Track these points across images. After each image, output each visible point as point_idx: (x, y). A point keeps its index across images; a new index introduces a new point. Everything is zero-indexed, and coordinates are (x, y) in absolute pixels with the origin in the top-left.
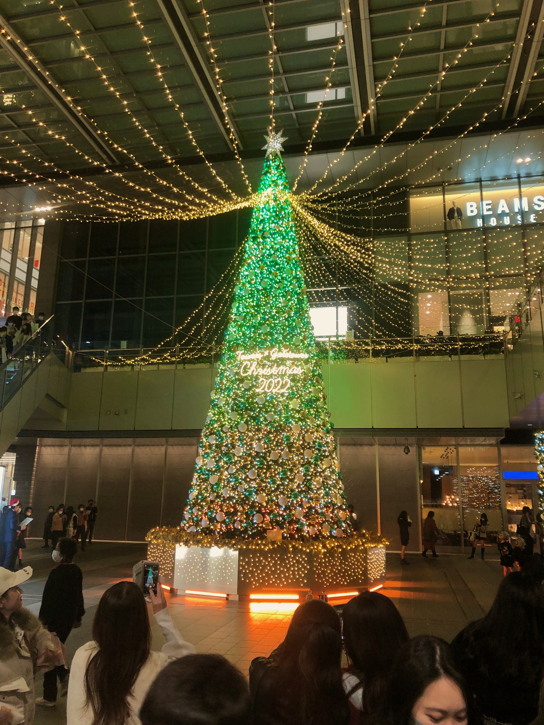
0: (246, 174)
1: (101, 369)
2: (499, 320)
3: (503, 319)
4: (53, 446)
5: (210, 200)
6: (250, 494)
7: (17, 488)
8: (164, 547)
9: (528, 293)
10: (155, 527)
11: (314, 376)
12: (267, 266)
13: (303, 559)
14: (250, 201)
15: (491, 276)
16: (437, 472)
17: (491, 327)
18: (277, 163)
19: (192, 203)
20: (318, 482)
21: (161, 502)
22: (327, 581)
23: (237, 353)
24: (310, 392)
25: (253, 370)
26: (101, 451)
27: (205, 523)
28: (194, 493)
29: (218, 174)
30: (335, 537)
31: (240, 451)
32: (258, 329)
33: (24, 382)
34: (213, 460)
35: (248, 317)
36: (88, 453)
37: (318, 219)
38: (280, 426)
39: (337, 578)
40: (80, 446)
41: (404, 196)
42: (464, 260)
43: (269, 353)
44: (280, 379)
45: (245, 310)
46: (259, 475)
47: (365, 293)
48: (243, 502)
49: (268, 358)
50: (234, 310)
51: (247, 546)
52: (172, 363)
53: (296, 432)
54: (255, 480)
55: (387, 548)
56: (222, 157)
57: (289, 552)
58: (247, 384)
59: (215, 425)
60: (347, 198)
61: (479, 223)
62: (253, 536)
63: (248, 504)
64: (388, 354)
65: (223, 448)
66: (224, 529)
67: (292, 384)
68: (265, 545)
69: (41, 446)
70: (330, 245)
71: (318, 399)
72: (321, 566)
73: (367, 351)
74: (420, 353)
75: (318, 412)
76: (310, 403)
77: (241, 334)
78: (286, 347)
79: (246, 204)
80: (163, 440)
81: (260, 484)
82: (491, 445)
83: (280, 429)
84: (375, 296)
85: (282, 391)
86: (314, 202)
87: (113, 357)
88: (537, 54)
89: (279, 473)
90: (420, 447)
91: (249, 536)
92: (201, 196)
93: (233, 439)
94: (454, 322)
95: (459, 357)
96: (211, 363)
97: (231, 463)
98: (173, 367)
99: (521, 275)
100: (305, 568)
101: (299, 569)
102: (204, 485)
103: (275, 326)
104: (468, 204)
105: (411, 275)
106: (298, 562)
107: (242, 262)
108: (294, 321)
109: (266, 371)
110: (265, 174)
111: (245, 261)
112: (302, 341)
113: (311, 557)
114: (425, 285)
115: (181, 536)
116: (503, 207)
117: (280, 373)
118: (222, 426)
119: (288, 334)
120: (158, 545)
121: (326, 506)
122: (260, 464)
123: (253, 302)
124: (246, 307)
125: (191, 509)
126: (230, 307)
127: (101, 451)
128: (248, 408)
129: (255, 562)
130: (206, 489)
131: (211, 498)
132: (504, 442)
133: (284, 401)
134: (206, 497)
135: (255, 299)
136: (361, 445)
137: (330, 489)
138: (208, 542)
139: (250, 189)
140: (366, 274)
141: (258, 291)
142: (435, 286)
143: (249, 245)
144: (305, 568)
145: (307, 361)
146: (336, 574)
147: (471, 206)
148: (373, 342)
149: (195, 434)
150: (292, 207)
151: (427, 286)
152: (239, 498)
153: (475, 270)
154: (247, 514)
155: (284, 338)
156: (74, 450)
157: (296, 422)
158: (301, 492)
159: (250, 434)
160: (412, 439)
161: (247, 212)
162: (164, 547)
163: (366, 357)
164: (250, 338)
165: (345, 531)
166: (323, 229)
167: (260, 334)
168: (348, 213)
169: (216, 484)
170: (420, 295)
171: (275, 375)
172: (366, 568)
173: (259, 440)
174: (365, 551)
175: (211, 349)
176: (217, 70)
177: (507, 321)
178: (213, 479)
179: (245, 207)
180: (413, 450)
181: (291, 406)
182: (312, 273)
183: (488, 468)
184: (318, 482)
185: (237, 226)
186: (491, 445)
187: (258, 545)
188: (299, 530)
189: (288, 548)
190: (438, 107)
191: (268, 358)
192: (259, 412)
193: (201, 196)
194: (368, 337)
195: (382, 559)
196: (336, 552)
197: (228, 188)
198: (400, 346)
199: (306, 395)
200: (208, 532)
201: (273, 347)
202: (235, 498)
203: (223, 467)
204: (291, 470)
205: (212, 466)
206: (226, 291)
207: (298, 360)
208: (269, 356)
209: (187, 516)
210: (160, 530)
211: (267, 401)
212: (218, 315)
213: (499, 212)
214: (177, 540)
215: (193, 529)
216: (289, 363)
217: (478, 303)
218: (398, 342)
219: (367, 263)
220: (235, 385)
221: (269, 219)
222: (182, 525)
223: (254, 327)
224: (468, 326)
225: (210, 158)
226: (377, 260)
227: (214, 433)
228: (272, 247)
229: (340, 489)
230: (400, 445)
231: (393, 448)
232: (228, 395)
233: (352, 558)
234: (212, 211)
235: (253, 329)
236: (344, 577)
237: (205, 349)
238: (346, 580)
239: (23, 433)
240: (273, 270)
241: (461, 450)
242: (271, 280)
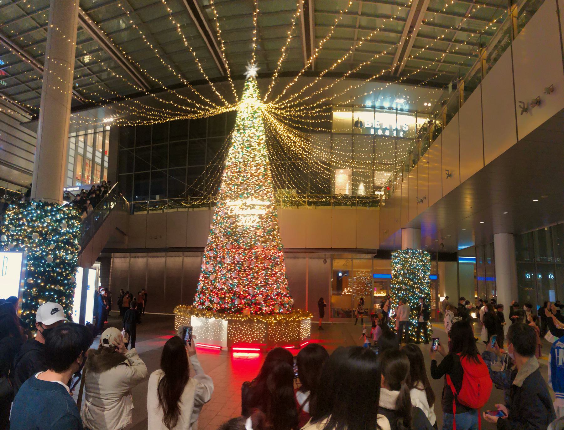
0: (235, 89)
1: (145, 212)
2: (379, 188)
3: (381, 188)
4: (121, 257)
5: (211, 106)
6: (234, 287)
7: (102, 282)
8: (184, 317)
9: (396, 176)
10: (179, 305)
11: (272, 215)
13: (263, 327)
14: (236, 107)
15: (377, 163)
16: (340, 274)
17: (374, 192)
18: (254, 83)
19: (200, 108)
20: (273, 280)
21: (181, 290)
22: (276, 340)
23: (226, 201)
24: (270, 225)
25: (236, 211)
26: (147, 260)
27: (207, 303)
28: (200, 286)
29: (217, 90)
30: (282, 313)
31: (228, 260)
32: (240, 186)
33: (105, 220)
35: (233, 179)
36: (140, 262)
37: (278, 119)
38: (251, 245)
39: (283, 338)
40: (135, 257)
41: (330, 110)
42: (363, 152)
45: (232, 174)
47: (305, 167)
48: (230, 291)
50: (225, 175)
51: (232, 318)
52: (185, 207)
53: (260, 250)
54: (236, 278)
55: (312, 319)
56: (220, 79)
57: (254, 322)
58: (232, 220)
59: (213, 245)
60: (297, 108)
61: (372, 132)
62: (235, 312)
63: (232, 293)
64: (316, 204)
65: (218, 259)
66: (219, 307)
67: (260, 220)
68: (242, 318)
69: (114, 257)
70: (284, 136)
71: (274, 230)
72: (273, 331)
73: (304, 201)
74: (335, 204)
75: (274, 237)
76: (269, 232)
77: (229, 189)
78: (256, 197)
79: (234, 109)
80: (181, 253)
82: (369, 259)
83: (251, 247)
84: (311, 169)
86: (276, 109)
87: (153, 205)
90: (332, 259)
91: (233, 312)
92: (205, 104)
94: (355, 187)
96: (209, 207)
98: (186, 210)
99: (393, 164)
100: (264, 332)
101: (260, 333)
105: (334, 158)
106: (260, 328)
107: (229, 145)
108: (261, 182)
109: (244, 212)
110: (246, 90)
111: (232, 144)
112: (266, 194)
113: (268, 325)
114: (341, 164)
115: (194, 311)
118: (217, 245)
119: (257, 190)
120: (181, 316)
121: (276, 295)
124: (232, 173)
125: (199, 295)
126: (222, 173)
127: (147, 260)
128: (233, 234)
129: (236, 328)
130: (207, 283)
131: (211, 288)
132: (375, 257)
133: (254, 231)
134: (208, 288)
136: (298, 258)
137: (280, 285)
138: (209, 315)
139: (237, 99)
140: (306, 155)
141: (240, 162)
142: (346, 165)
143: (235, 134)
144: (264, 332)
145: (268, 207)
146: (282, 336)
148: (308, 196)
149: (200, 250)
150: (262, 112)
151: (341, 165)
153: (369, 158)
154: (231, 298)
155: (255, 192)
156: (132, 260)
157: (261, 243)
158: (262, 286)
159: (234, 250)
160: (328, 255)
161: (234, 113)
162: (184, 317)
163: (303, 205)
164: (234, 192)
165: (288, 310)
166: (280, 128)
167: (241, 189)
168: (297, 117)
169: (214, 280)
170: (337, 170)
172: (299, 331)
173: (239, 254)
174: (299, 322)
175: (209, 199)
176: (218, 24)
177: (383, 189)
178: (212, 278)
179: (233, 111)
180: (328, 261)
181: (258, 234)
182: (273, 153)
183: (367, 272)
184: (273, 280)
185: (227, 122)
186: (369, 259)
187: (238, 317)
188: (261, 309)
189: (254, 320)
192: (239, 237)
193: (205, 104)
194: (305, 193)
195: (309, 326)
196: (282, 322)
197: (223, 98)
198: (324, 200)
199: (267, 227)
200: (209, 309)
201: (248, 197)
203: (218, 270)
204: (257, 273)
205: (211, 269)
206: (219, 163)
207: (263, 206)
208: (245, 203)
209: (197, 299)
210: (182, 307)
211: (244, 230)
212: (214, 178)
214: (192, 313)
215: (201, 307)
216: (257, 207)
217: (368, 178)
218: (323, 197)
219: (307, 148)
221: (247, 118)
222: (194, 304)
223: (237, 185)
224: (361, 190)
225: (212, 80)
226: (313, 147)
227: (213, 250)
228: (249, 136)
229: (286, 284)
230: (321, 258)
231: (317, 260)
232: (221, 227)
233: (292, 326)
234: (211, 113)
236: (286, 337)
237: (206, 198)
238: (288, 339)
239: (105, 250)
240: (249, 150)
241: (354, 261)
242: (248, 156)
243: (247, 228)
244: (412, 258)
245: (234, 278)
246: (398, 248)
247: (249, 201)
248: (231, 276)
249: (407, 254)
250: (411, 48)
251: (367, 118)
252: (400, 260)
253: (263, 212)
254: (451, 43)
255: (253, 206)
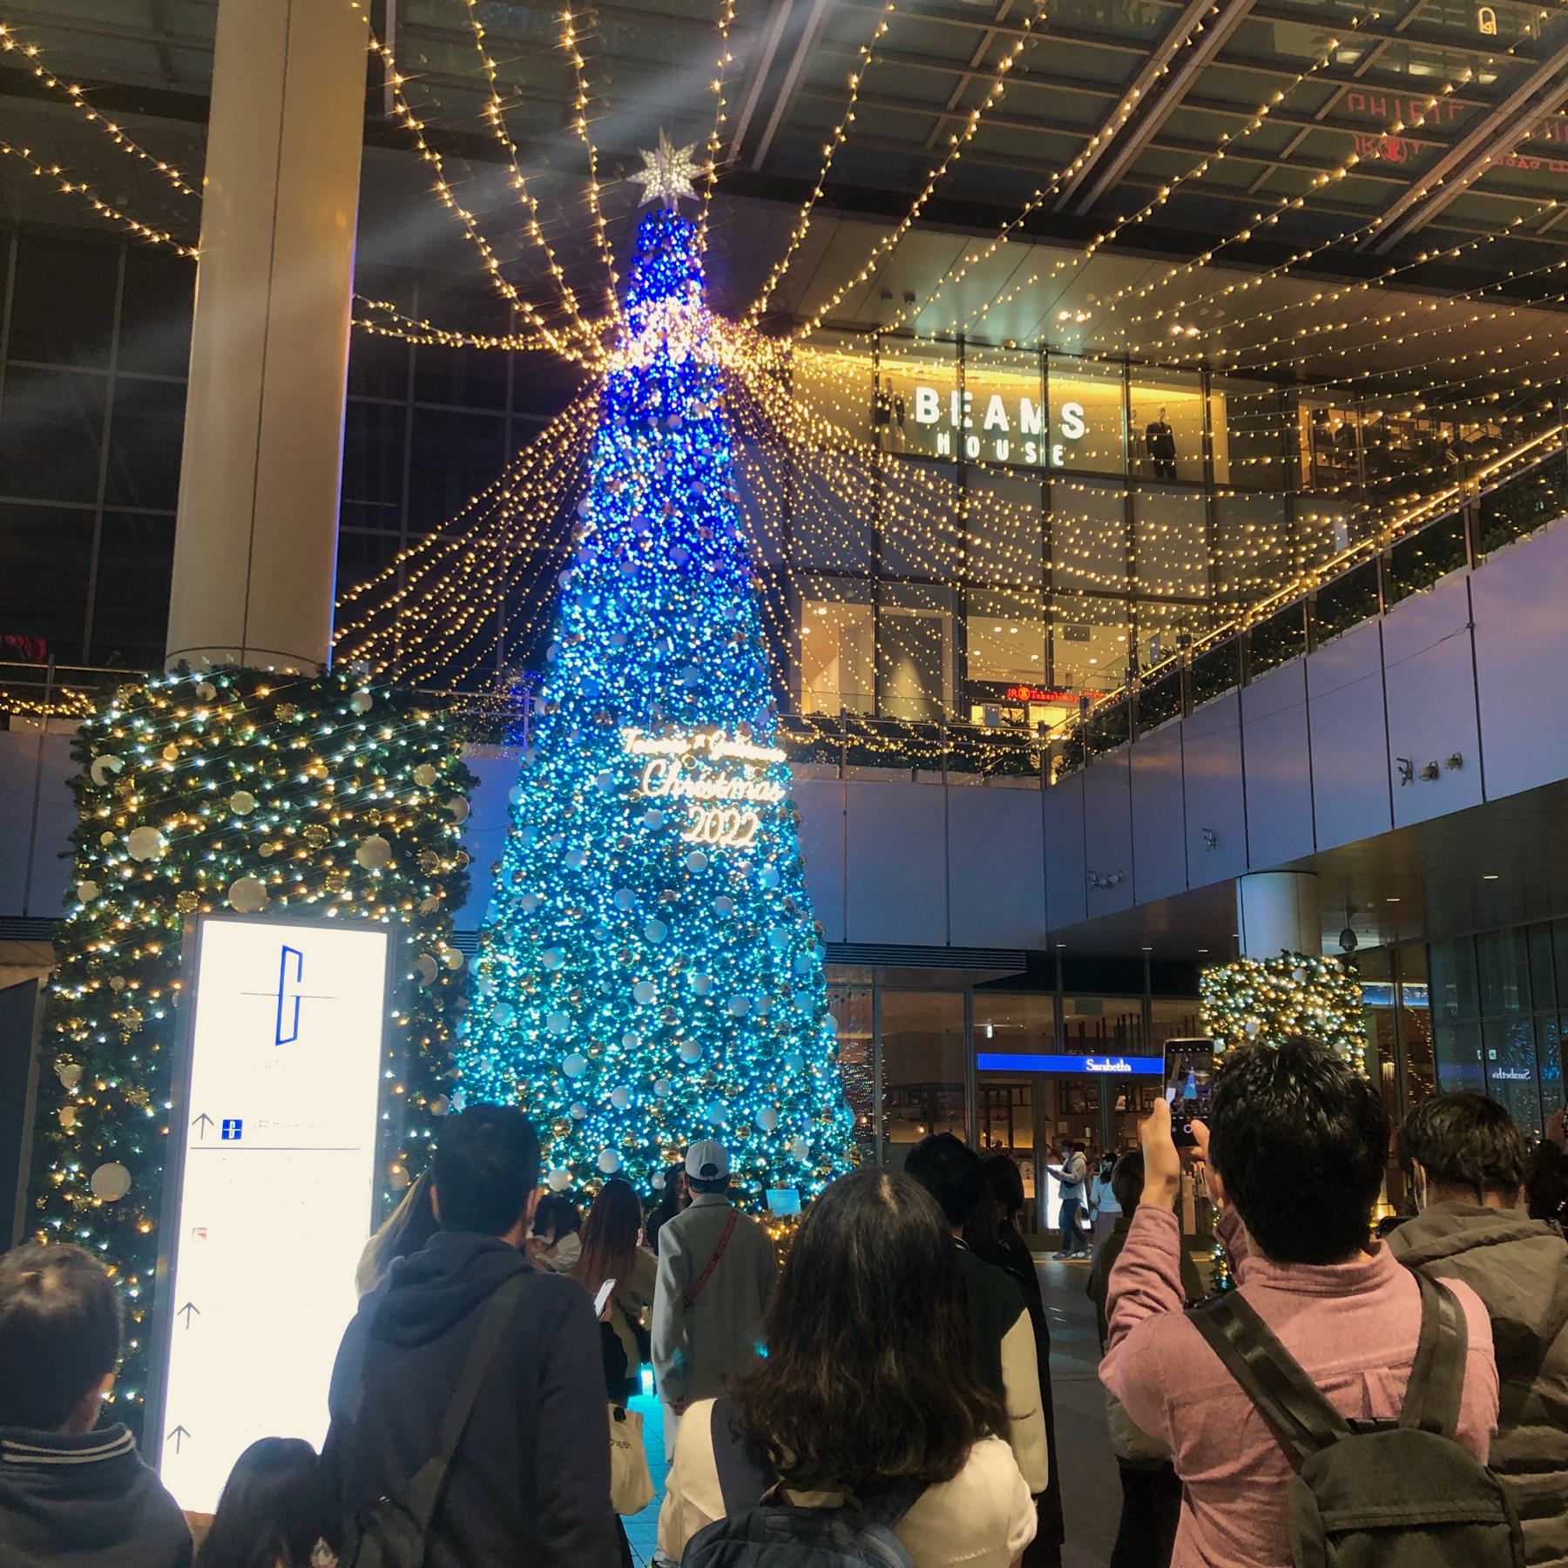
12: (682, 507)
25: (673, 784)
34: (565, 1013)
43: (707, 742)
44: (734, 811)
46: (706, 1055)
49: (702, 753)
54: (696, 1066)
63: (685, 1129)
81: (711, 1076)
85: (739, 844)
88: (1184, 92)
89: (752, 1051)
93: (627, 961)
95: (944, 777)
97: (628, 1022)
102: (537, 1079)
103: (713, 672)
104: (921, 392)
116: (996, 416)
117: (733, 797)
122: (707, 1027)
123: (651, 598)
135: (658, 594)
147: (927, 398)
152: (660, 1112)
157: (778, 924)
167: (679, 690)
171: (723, 801)
173: (699, 964)
190: (930, 145)
191: (702, 753)
202: (649, 1112)
211: (711, 865)
213: (988, 426)
220: (617, 819)
224: (906, 699)
235: (658, 675)
243: (721, 857)
244: (1305, 990)
245: (689, 1066)
246: (1227, 951)
247: (719, 746)
248: (677, 1058)
249: (1286, 973)
250: (1176, 104)
251: (927, 387)
252: (1256, 998)
253: (774, 793)
254: (993, 31)
255: (731, 767)
